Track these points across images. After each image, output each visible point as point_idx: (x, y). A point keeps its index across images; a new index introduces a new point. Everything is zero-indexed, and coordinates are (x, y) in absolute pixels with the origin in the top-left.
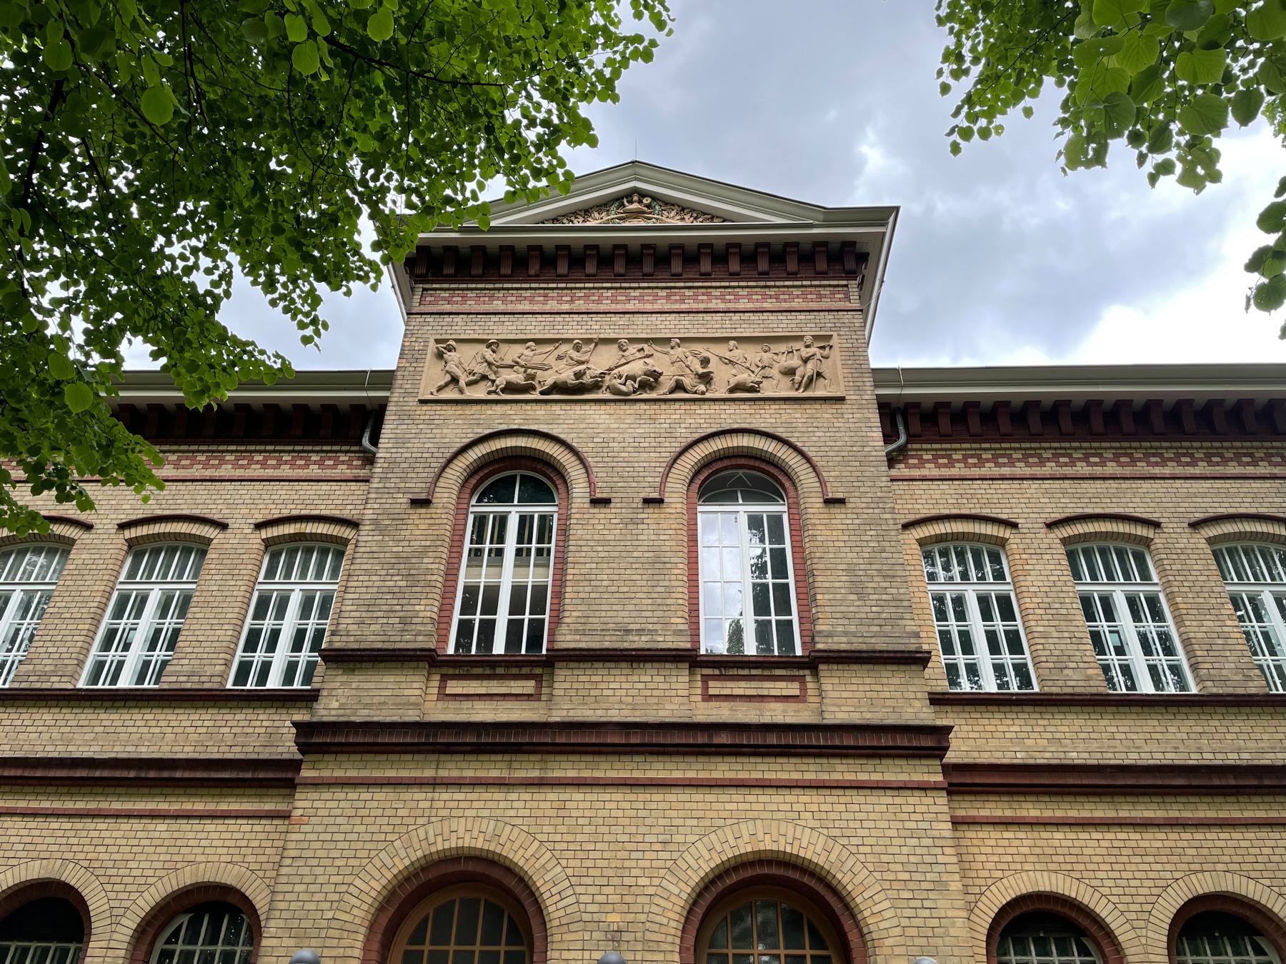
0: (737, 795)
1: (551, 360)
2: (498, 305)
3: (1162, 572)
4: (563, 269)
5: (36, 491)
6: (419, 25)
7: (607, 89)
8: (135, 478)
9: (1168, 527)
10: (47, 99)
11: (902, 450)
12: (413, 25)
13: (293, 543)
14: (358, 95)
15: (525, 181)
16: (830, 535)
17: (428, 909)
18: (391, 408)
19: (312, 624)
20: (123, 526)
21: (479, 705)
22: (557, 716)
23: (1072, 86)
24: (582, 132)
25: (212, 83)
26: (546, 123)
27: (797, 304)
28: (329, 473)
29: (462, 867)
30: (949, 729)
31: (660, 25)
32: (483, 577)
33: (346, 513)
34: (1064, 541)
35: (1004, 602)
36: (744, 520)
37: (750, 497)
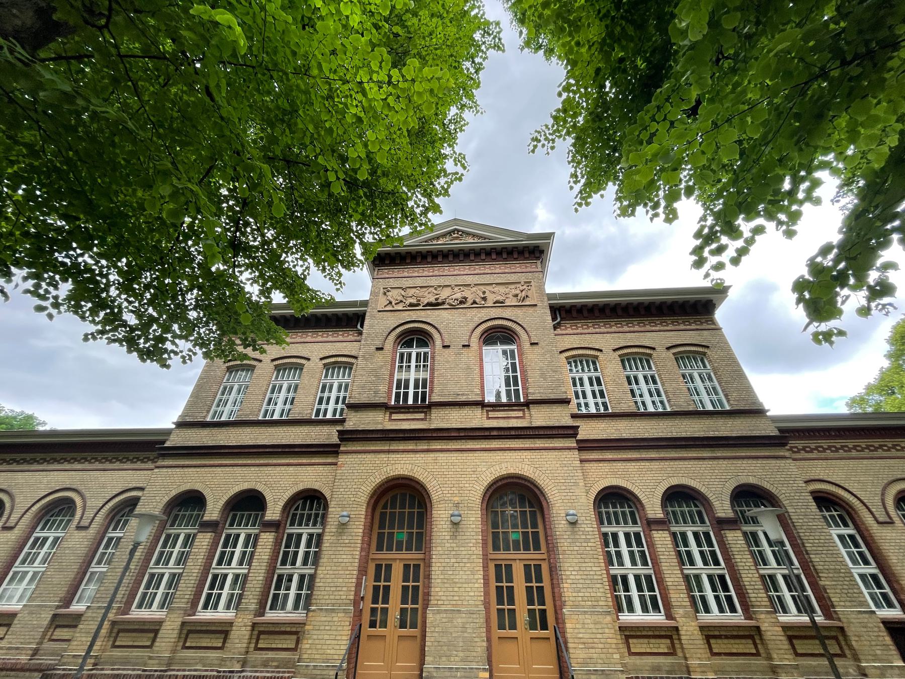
0: (500, 453)
1: (426, 294)
2: (406, 274)
3: (656, 366)
4: (429, 260)
5: (245, 348)
6: (375, 172)
7: (446, 192)
8: (279, 342)
9: (658, 349)
10: (241, 205)
11: (559, 324)
12: (373, 172)
13: (334, 365)
14: (354, 199)
15: (416, 227)
16: (533, 357)
17: (388, 497)
18: (367, 314)
19: (342, 394)
20: (273, 360)
21: (404, 423)
22: (433, 426)
23: (619, 185)
24: (436, 209)
25: (301, 197)
26: (423, 206)
27: (518, 270)
28: (346, 339)
29: (400, 481)
30: (578, 427)
31: (465, 168)
32: (403, 376)
33: (353, 354)
34: (620, 356)
35: (598, 379)
36: (500, 352)
37: (502, 343)
